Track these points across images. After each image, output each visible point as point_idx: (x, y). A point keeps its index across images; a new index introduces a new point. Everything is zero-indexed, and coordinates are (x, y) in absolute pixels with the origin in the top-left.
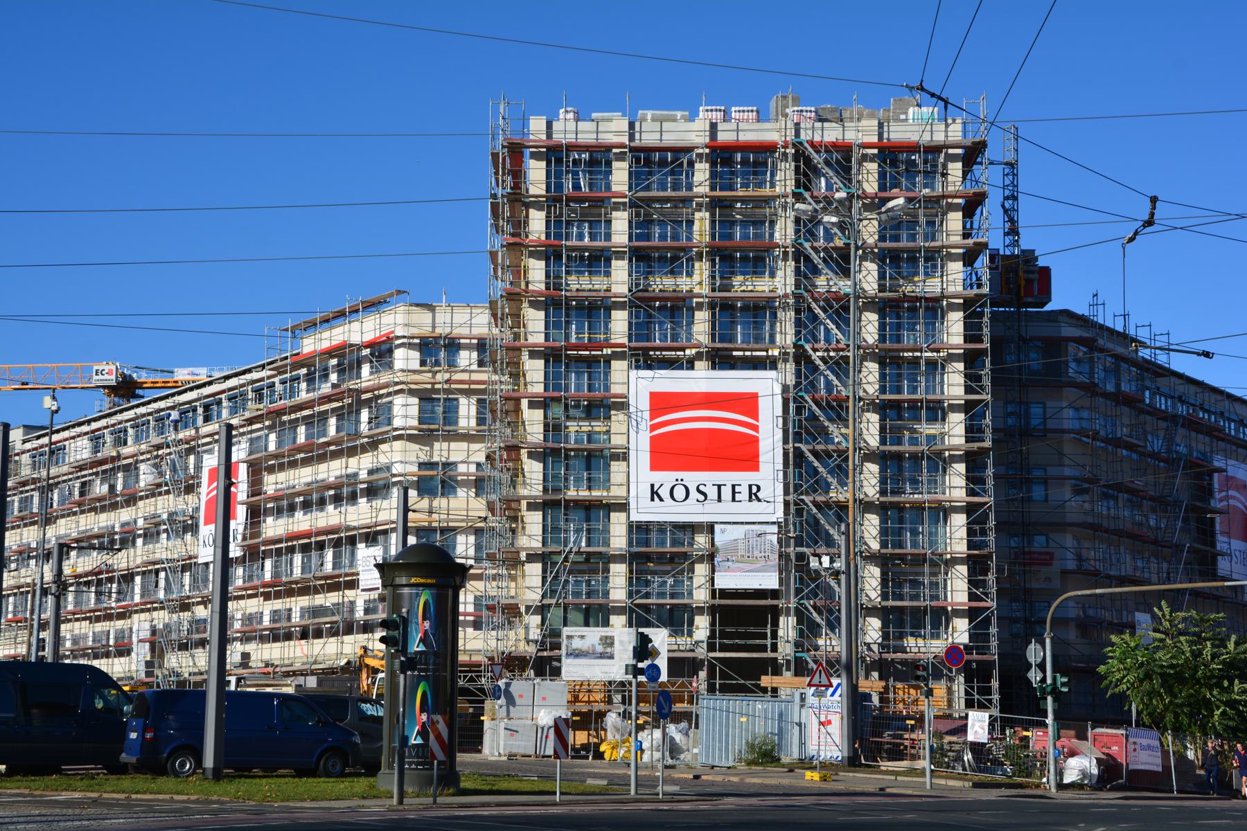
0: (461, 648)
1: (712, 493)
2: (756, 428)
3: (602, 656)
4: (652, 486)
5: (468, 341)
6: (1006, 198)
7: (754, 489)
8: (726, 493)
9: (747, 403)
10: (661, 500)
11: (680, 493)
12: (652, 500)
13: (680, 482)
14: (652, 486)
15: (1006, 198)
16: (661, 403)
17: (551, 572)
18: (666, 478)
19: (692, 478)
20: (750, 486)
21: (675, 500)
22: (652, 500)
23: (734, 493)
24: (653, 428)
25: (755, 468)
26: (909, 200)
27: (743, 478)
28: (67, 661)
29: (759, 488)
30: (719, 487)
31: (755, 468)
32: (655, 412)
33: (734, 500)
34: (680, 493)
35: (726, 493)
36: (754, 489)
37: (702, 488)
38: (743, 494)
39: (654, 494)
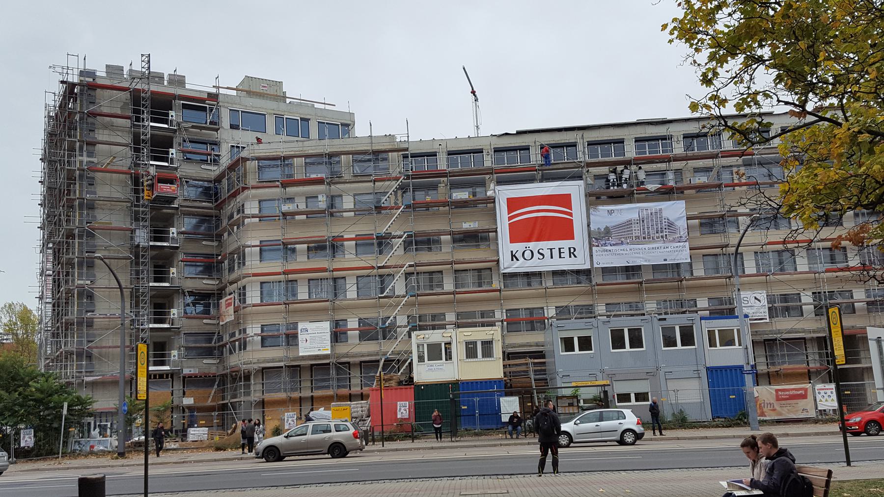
0: (840, 422)
1: (547, 253)
2: (571, 214)
3: (666, 372)
4: (512, 252)
5: (712, 189)
6: (851, 35)
7: (572, 250)
8: (556, 253)
9: (564, 200)
10: (517, 260)
11: (528, 254)
12: (512, 260)
13: (528, 249)
14: (512, 252)
15: (851, 35)
16: (514, 204)
17: (799, 351)
18: (519, 247)
19: (533, 245)
20: (570, 248)
21: (525, 259)
22: (512, 260)
23: (560, 253)
24: (510, 219)
25: (572, 237)
26: (76, 94)
27: (565, 244)
28: (845, 495)
29: (575, 250)
30: (551, 250)
31: (572, 237)
32: (510, 210)
33: (560, 257)
34: (528, 254)
35: (556, 253)
36: (572, 250)
37: (540, 251)
38: (566, 254)
39: (513, 256)
